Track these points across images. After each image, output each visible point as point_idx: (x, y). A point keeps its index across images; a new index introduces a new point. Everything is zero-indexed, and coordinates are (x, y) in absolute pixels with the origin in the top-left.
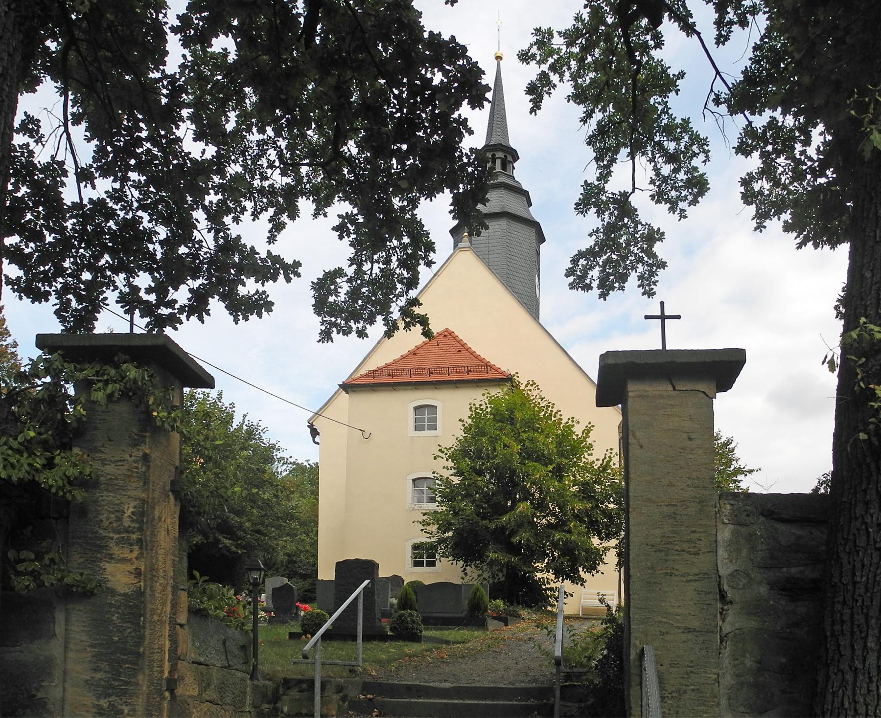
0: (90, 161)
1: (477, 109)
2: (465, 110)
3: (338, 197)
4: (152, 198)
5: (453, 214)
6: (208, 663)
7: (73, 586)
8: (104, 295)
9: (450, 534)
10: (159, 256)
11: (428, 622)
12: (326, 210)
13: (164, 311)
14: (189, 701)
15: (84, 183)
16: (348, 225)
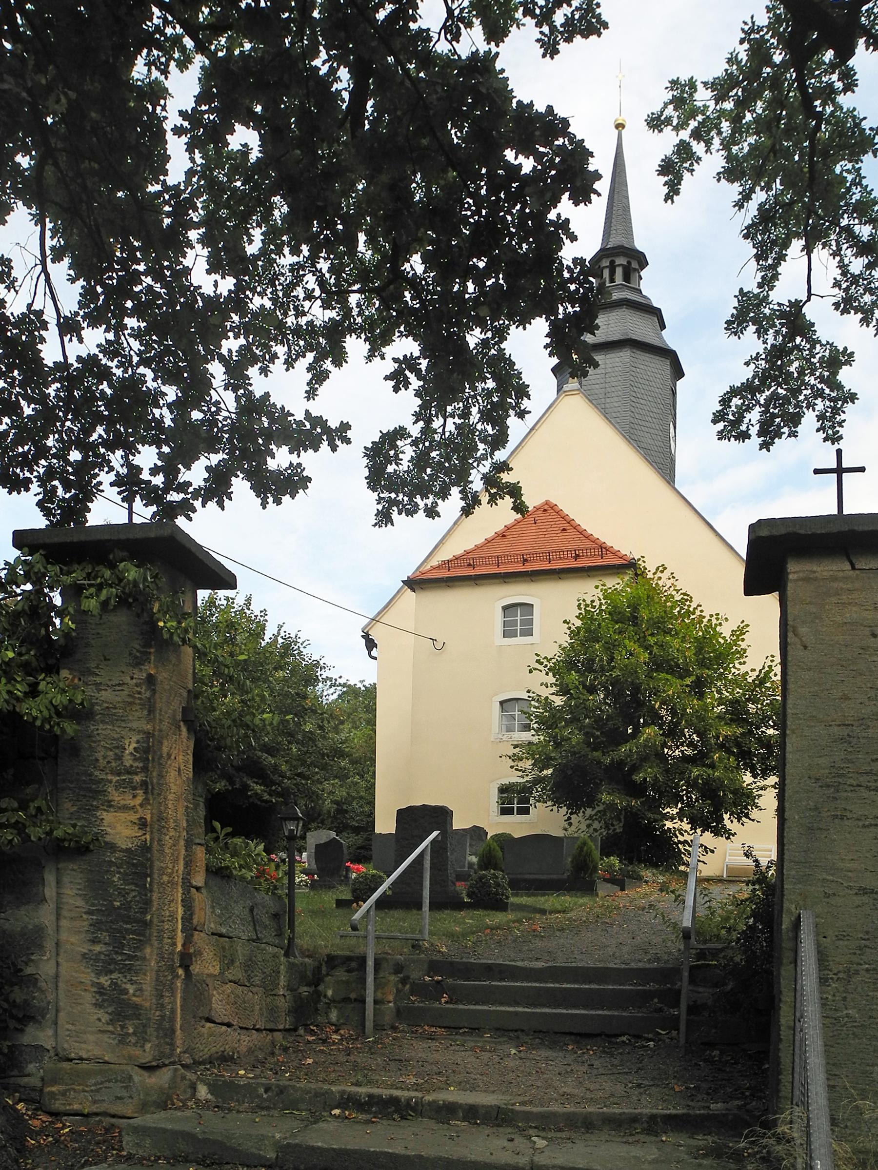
0: (75, 308)
1: (582, 205)
2: (565, 208)
3: (399, 332)
4: (156, 349)
5: (549, 349)
6: (231, 935)
7: (65, 840)
8: (98, 479)
10: (168, 422)
11: (518, 885)
12: (383, 350)
13: (174, 497)
14: (209, 981)
15: (69, 336)
16: (407, 372)
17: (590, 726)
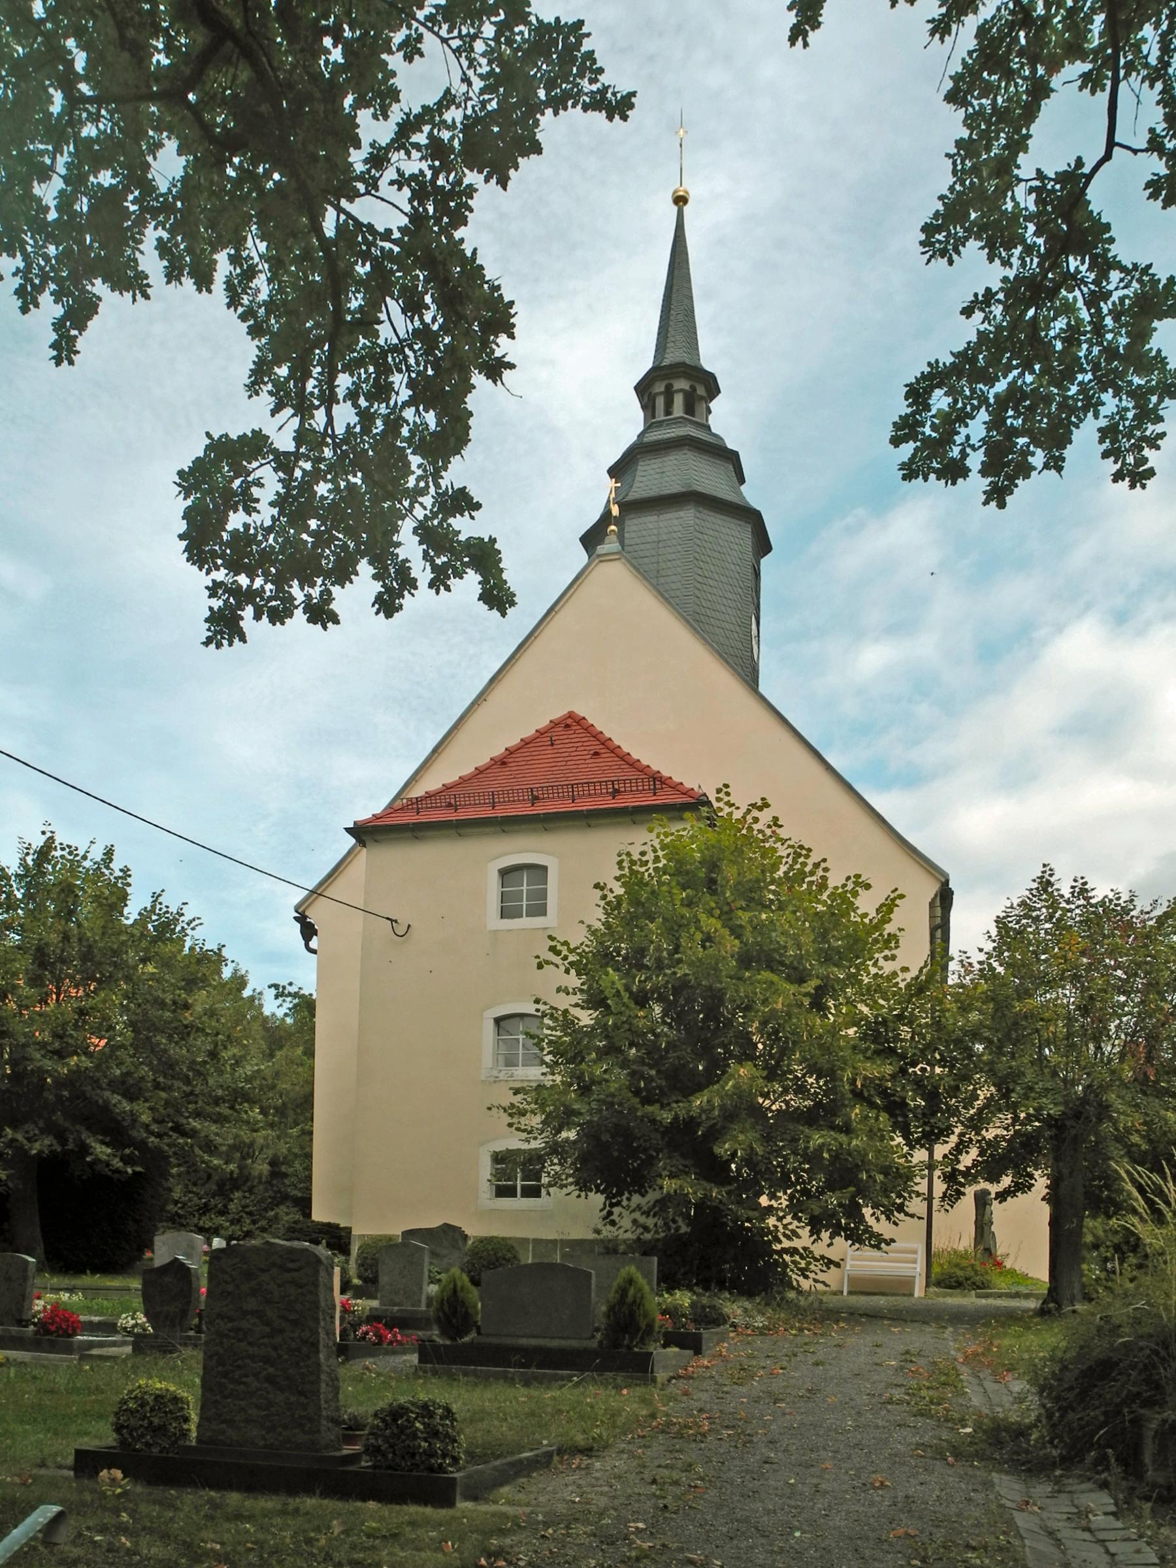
9: (571, 1135)
17: (641, 1061)
